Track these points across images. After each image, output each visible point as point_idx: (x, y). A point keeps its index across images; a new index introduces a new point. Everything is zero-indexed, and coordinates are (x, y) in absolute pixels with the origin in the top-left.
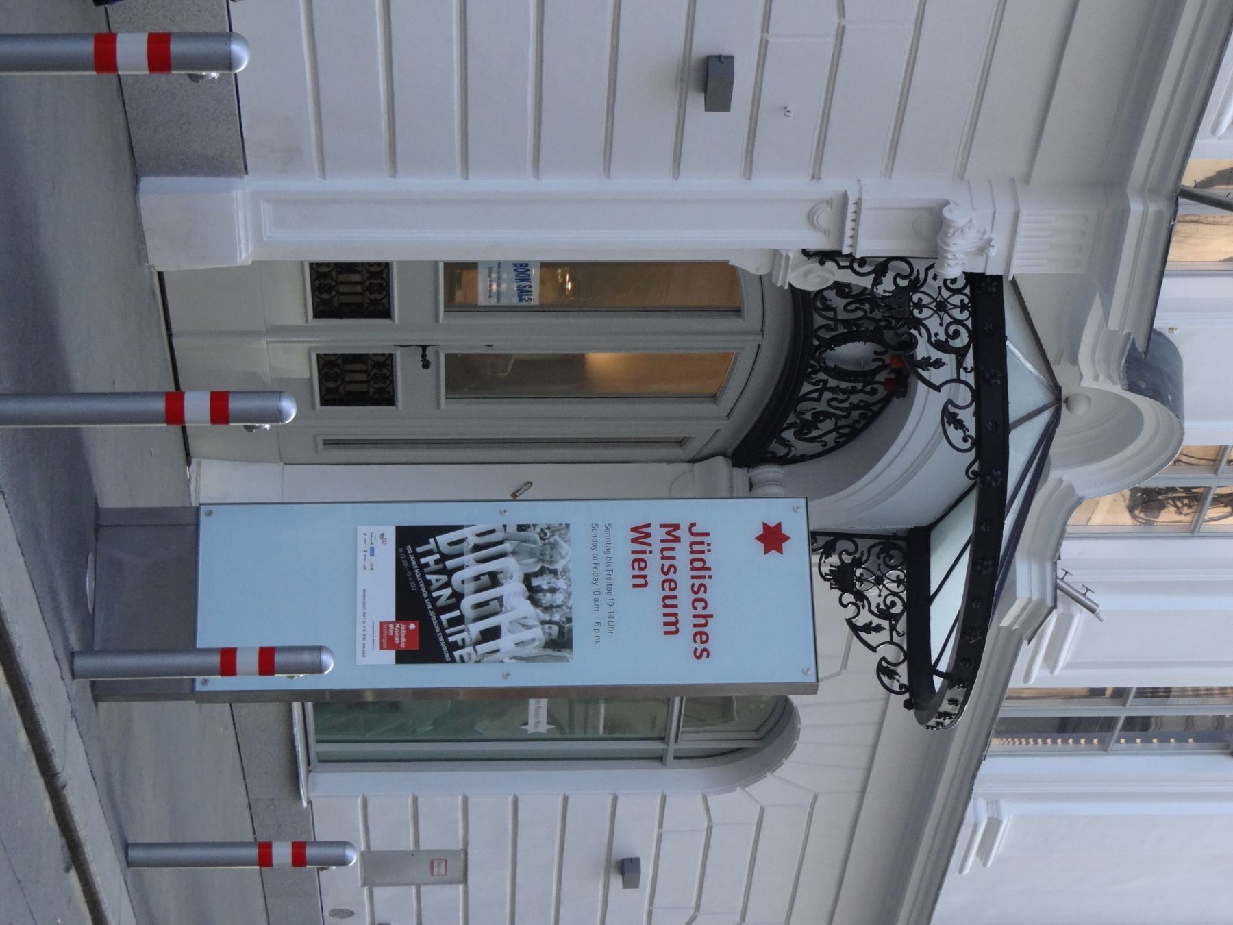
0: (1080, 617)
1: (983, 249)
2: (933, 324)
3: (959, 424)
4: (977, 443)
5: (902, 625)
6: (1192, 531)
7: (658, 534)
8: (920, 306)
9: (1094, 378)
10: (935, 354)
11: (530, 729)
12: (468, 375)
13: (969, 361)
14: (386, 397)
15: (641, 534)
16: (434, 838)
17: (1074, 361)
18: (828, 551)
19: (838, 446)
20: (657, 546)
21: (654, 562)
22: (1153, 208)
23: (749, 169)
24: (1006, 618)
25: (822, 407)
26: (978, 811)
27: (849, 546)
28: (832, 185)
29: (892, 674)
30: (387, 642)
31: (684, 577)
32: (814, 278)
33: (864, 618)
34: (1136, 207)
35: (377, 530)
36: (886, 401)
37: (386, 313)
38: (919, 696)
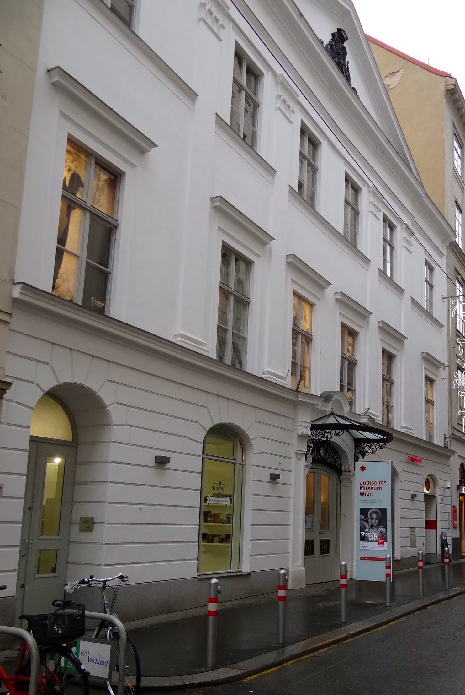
0: (369, 411)
1: (306, 427)
2: (320, 437)
3: (339, 433)
4: (342, 429)
6: (309, 369)
7: (362, 491)
8: (316, 439)
9: (329, 408)
10: (325, 437)
12: (324, 526)
13: (327, 430)
14: (328, 541)
15: (362, 494)
16: (407, 533)
18: (358, 458)
21: (367, 491)
22: (300, 396)
24: (371, 425)
25: (332, 458)
26: (403, 430)
28: (293, 455)
29: (382, 446)
31: (370, 486)
32: (310, 459)
34: (300, 399)
36: (331, 446)
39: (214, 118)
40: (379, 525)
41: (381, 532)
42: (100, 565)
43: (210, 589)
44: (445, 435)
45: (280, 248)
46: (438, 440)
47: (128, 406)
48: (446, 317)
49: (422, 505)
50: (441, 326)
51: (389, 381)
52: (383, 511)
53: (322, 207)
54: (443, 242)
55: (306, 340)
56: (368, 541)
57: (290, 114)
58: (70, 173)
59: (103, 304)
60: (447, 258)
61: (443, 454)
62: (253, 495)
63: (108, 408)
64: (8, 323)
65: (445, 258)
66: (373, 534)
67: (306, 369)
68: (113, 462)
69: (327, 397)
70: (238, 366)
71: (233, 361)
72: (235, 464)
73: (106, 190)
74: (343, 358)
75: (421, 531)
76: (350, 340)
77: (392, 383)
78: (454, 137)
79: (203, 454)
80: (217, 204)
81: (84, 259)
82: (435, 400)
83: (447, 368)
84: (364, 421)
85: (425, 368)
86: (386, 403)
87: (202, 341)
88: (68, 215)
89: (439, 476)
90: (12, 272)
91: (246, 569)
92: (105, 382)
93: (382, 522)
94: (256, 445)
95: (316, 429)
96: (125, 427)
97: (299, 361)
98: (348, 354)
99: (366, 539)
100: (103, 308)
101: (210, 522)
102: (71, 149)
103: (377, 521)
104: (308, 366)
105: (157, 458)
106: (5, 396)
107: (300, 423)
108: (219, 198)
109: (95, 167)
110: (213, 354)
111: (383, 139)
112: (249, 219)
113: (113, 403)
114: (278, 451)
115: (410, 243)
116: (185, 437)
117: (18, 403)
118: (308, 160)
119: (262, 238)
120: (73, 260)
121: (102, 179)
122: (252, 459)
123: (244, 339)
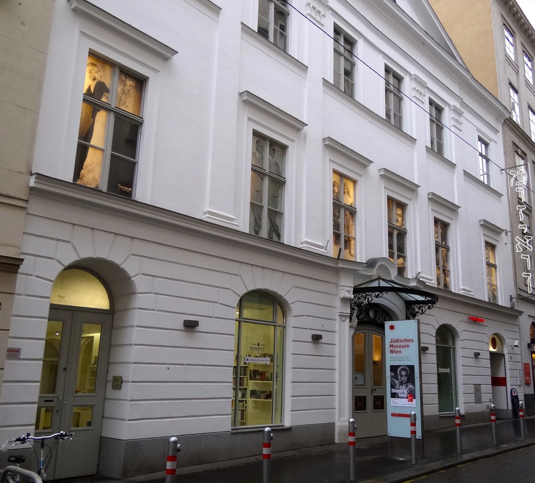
1: (348, 291)
3: (378, 295)
4: (381, 292)
5: (422, 305)
6: (355, 239)
7: (392, 349)
9: (374, 273)
10: (367, 299)
11: (449, 372)
13: (368, 293)
15: (392, 352)
16: (472, 389)
17: (371, 276)
21: (396, 349)
23: (336, 332)
26: (462, 292)
28: (337, 317)
30: (411, 400)
31: (399, 344)
32: (355, 321)
33: (420, 312)
34: (340, 266)
35: (392, 402)
36: (381, 308)
37: (365, 397)
38: (433, 302)
39: (240, 26)
40: (408, 382)
41: (410, 389)
42: (124, 420)
43: (169, 446)
44: (511, 296)
45: (315, 133)
46: (503, 301)
47: (154, 276)
48: (505, 187)
49: (488, 363)
50: (500, 195)
51: (444, 248)
52: (412, 368)
53: (360, 95)
54: (497, 119)
55: (350, 213)
56: (399, 397)
57: (321, 18)
58: (95, 82)
59: (130, 189)
60: (504, 134)
61: (511, 314)
62: (293, 354)
63: (132, 279)
64: (26, 208)
65: (500, 135)
66: (403, 391)
67: (351, 239)
68: (138, 326)
69: (371, 264)
70: (275, 238)
71: (270, 234)
72: (275, 326)
73: (133, 92)
74: (391, 229)
75: (487, 388)
76: (399, 212)
77: (448, 249)
78: (504, 27)
79: (240, 317)
80: (245, 98)
81: (109, 152)
82: (497, 264)
83: (509, 234)
84: (413, 284)
85: (483, 234)
86: (442, 268)
87: (233, 217)
88: (94, 116)
89: (506, 335)
90: (29, 165)
91: (287, 423)
92: (129, 256)
93: (411, 379)
94: (295, 309)
95: (359, 293)
96: (152, 295)
97: (342, 231)
98: (398, 224)
99: (396, 396)
100: (131, 192)
101: (258, 380)
102: (94, 62)
103: (406, 379)
104: (354, 236)
105: (185, 322)
106: (19, 271)
107: (341, 288)
108: (246, 93)
109: (120, 75)
110: (246, 229)
111: (421, 32)
112: (278, 109)
113: (138, 274)
114: (320, 315)
115: (459, 122)
116: (216, 303)
117: (37, 276)
118: (344, 56)
119: (296, 125)
120: (99, 153)
121: (128, 85)
122: (291, 321)
123: (281, 214)
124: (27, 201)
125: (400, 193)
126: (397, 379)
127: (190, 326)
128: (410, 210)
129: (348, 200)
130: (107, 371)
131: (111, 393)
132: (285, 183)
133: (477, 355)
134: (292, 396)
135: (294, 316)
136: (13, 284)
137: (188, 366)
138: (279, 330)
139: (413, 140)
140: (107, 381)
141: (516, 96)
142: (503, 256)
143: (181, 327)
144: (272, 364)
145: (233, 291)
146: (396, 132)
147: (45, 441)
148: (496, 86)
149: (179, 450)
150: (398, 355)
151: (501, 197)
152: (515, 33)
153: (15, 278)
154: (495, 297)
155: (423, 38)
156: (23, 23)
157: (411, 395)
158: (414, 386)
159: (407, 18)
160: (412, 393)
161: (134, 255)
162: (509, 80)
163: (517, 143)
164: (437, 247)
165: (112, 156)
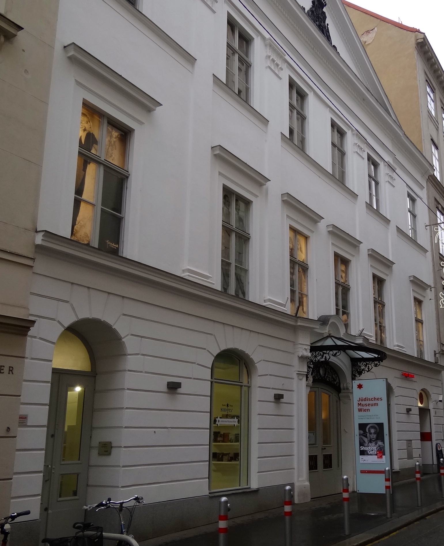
0: (364, 332)
1: (306, 349)
2: (319, 358)
3: (336, 353)
4: (339, 350)
6: (307, 296)
7: (360, 407)
8: (315, 360)
9: (326, 330)
10: (324, 357)
12: (326, 441)
13: (325, 352)
14: (330, 456)
15: (360, 410)
18: (355, 376)
19: (337, 374)
20: (362, 407)
21: (365, 408)
23: (294, 391)
27: (354, 372)
28: (295, 376)
29: (377, 364)
30: (381, 457)
31: (367, 402)
32: (311, 379)
33: (367, 369)
34: (299, 324)
39: (212, 78)
40: (377, 439)
41: (379, 446)
42: (118, 487)
44: (435, 351)
45: (275, 189)
46: (429, 357)
47: (142, 337)
50: (426, 251)
52: (381, 425)
53: (312, 150)
54: (423, 176)
56: (368, 455)
58: (86, 133)
62: (259, 414)
63: (123, 340)
64: (32, 267)
65: (425, 190)
66: (372, 448)
67: (303, 296)
70: (241, 296)
71: (236, 291)
72: (241, 386)
73: (118, 144)
74: (337, 284)
75: (417, 443)
76: (343, 268)
77: (383, 306)
78: (427, 83)
79: (212, 378)
81: (99, 207)
82: (423, 319)
83: (433, 289)
84: (360, 341)
90: (34, 221)
91: (254, 485)
93: (380, 436)
94: (261, 368)
97: (297, 288)
98: (342, 281)
100: (118, 249)
101: (219, 442)
103: (375, 436)
104: (306, 293)
106: (30, 333)
109: (108, 126)
110: (218, 286)
112: (246, 164)
113: (128, 335)
114: (280, 373)
115: (392, 178)
116: (194, 363)
117: (41, 339)
120: (90, 207)
121: (114, 136)
124: (33, 259)
125: (342, 247)
126: (366, 437)
127: (173, 387)
128: (353, 266)
129: (301, 256)
130: (91, 437)
131: (95, 458)
132: (249, 239)
133: (409, 410)
134: (258, 458)
135: (259, 376)
136: (23, 346)
137: (173, 430)
138: (245, 389)
139: (355, 196)
140: (91, 447)
141: (436, 151)
142: (429, 313)
143: (165, 389)
144: (239, 425)
145: (208, 351)
146: (339, 186)
147: (124, 505)
148: (421, 142)
149: (229, 510)
150: (367, 413)
151: (426, 253)
152: (435, 89)
153: (26, 341)
154: (421, 352)
155: (364, 94)
156: (26, 71)
157: (381, 452)
158: (384, 443)
159: (351, 74)
160: (381, 450)
161: (124, 315)
162: (431, 136)
163: (438, 199)
164: (375, 302)
165: (102, 210)
